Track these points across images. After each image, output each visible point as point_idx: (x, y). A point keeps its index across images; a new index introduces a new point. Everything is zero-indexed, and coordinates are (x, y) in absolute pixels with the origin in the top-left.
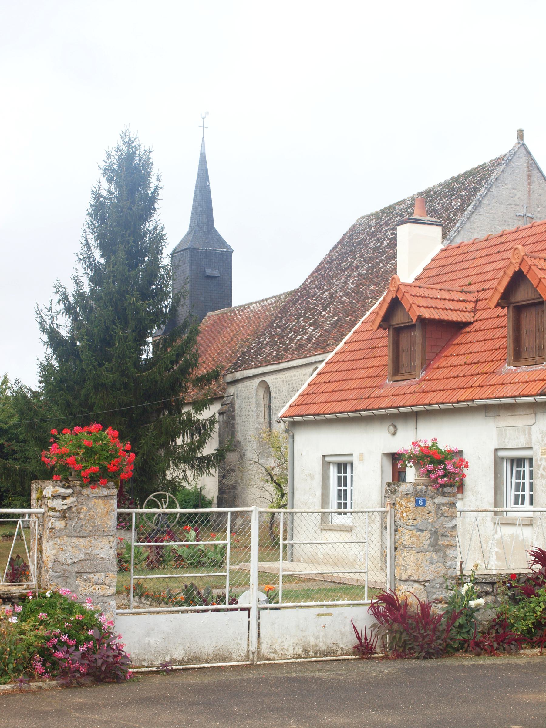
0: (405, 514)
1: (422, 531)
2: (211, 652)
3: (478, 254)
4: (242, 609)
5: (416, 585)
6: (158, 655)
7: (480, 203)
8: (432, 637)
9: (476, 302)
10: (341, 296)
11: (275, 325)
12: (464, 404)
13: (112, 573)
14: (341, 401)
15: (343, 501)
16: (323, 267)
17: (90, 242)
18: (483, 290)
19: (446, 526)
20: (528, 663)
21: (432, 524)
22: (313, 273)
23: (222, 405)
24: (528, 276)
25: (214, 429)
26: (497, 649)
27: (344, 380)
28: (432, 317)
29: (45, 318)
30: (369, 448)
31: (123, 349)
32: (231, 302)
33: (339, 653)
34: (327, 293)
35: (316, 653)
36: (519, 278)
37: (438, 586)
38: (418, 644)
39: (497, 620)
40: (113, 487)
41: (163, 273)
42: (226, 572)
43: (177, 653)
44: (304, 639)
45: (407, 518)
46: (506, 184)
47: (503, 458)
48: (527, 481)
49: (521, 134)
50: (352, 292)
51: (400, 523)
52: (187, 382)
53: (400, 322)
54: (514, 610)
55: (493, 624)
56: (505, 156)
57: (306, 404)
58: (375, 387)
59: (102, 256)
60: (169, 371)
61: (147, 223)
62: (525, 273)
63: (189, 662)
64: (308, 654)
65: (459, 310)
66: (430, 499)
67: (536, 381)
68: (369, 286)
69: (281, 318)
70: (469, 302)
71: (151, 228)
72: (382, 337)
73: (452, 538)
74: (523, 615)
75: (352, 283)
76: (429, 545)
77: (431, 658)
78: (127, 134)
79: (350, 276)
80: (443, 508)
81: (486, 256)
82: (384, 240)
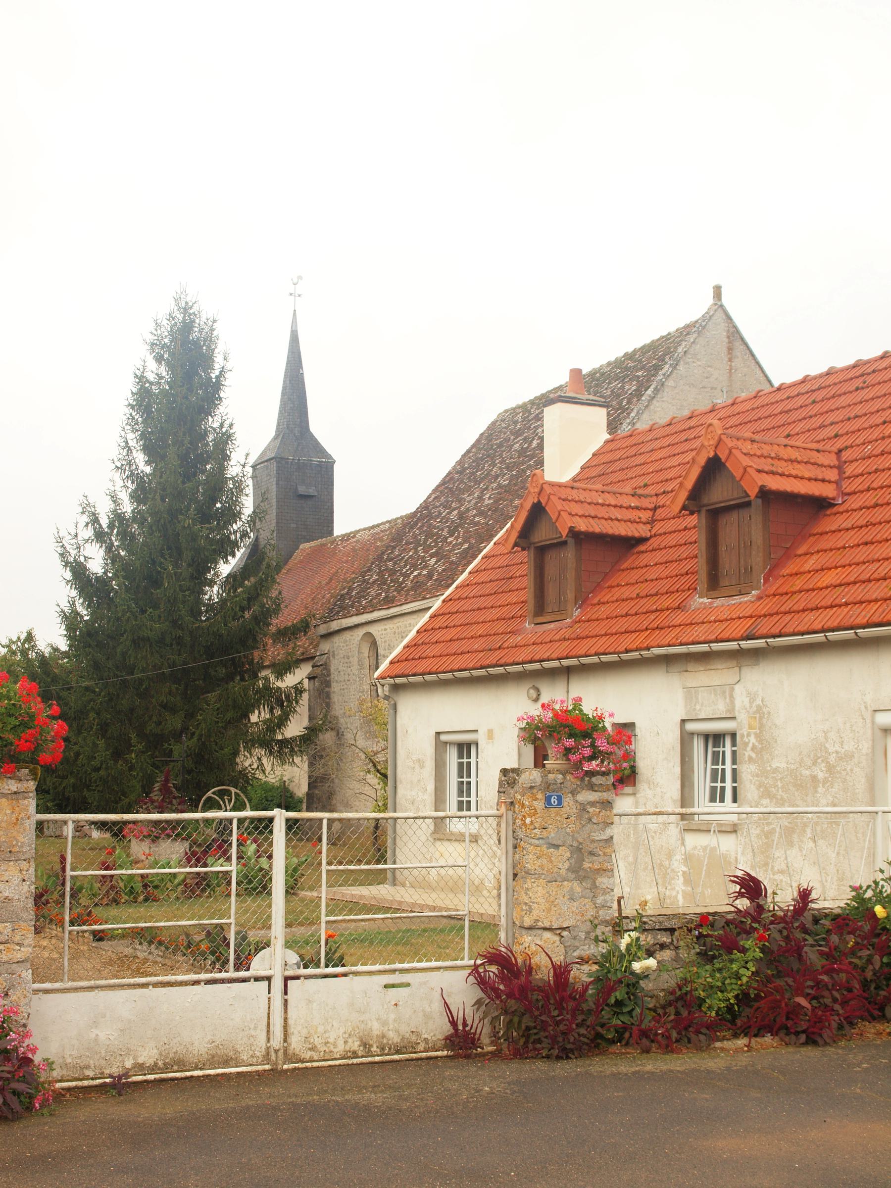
0: (528, 821)
1: (557, 847)
2: (203, 1051)
3: (657, 444)
4: (257, 979)
5: (547, 935)
6: (112, 1059)
7: (663, 385)
8: (571, 1023)
9: (655, 509)
10: (474, 516)
11: (385, 557)
12: (635, 655)
13: (25, 924)
14: (462, 653)
15: (465, 799)
16: (452, 479)
17: (131, 443)
18: (664, 492)
19: (597, 838)
20: (728, 1068)
21: (573, 836)
22: (438, 487)
23: (313, 667)
24: (727, 464)
25: (301, 702)
26: (677, 1041)
27: (467, 624)
28: (591, 530)
29: (68, 547)
30: (498, 721)
31: (175, 591)
32: (332, 530)
33: (421, 1047)
34: (455, 512)
35: (383, 1049)
36: (714, 468)
37: (582, 935)
38: (547, 1034)
39: (679, 993)
40: (28, 778)
41: (231, 486)
42: (229, 918)
43: (145, 1054)
44: (362, 1026)
45: (532, 827)
46: (698, 360)
47: (692, 734)
48: (728, 767)
49: (718, 292)
50: (489, 510)
51: (520, 834)
52: (265, 635)
53: (544, 538)
54: (705, 975)
55: (672, 998)
56: (696, 322)
57: (413, 659)
58: (510, 632)
59: (148, 463)
60: (238, 620)
61: (210, 418)
62: (723, 460)
63: (167, 1068)
64: (370, 1051)
65: (629, 521)
66: (570, 795)
67: (740, 618)
68: (512, 501)
69: (394, 548)
70: (644, 509)
71: (216, 425)
72: (521, 563)
73: (606, 858)
74: (719, 984)
75: (489, 498)
76: (568, 870)
77: (568, 1058)
78: (183, 296)
79: (486, 489)
80: (591, 810)
81: (669, 446)
82: (533, 439)
